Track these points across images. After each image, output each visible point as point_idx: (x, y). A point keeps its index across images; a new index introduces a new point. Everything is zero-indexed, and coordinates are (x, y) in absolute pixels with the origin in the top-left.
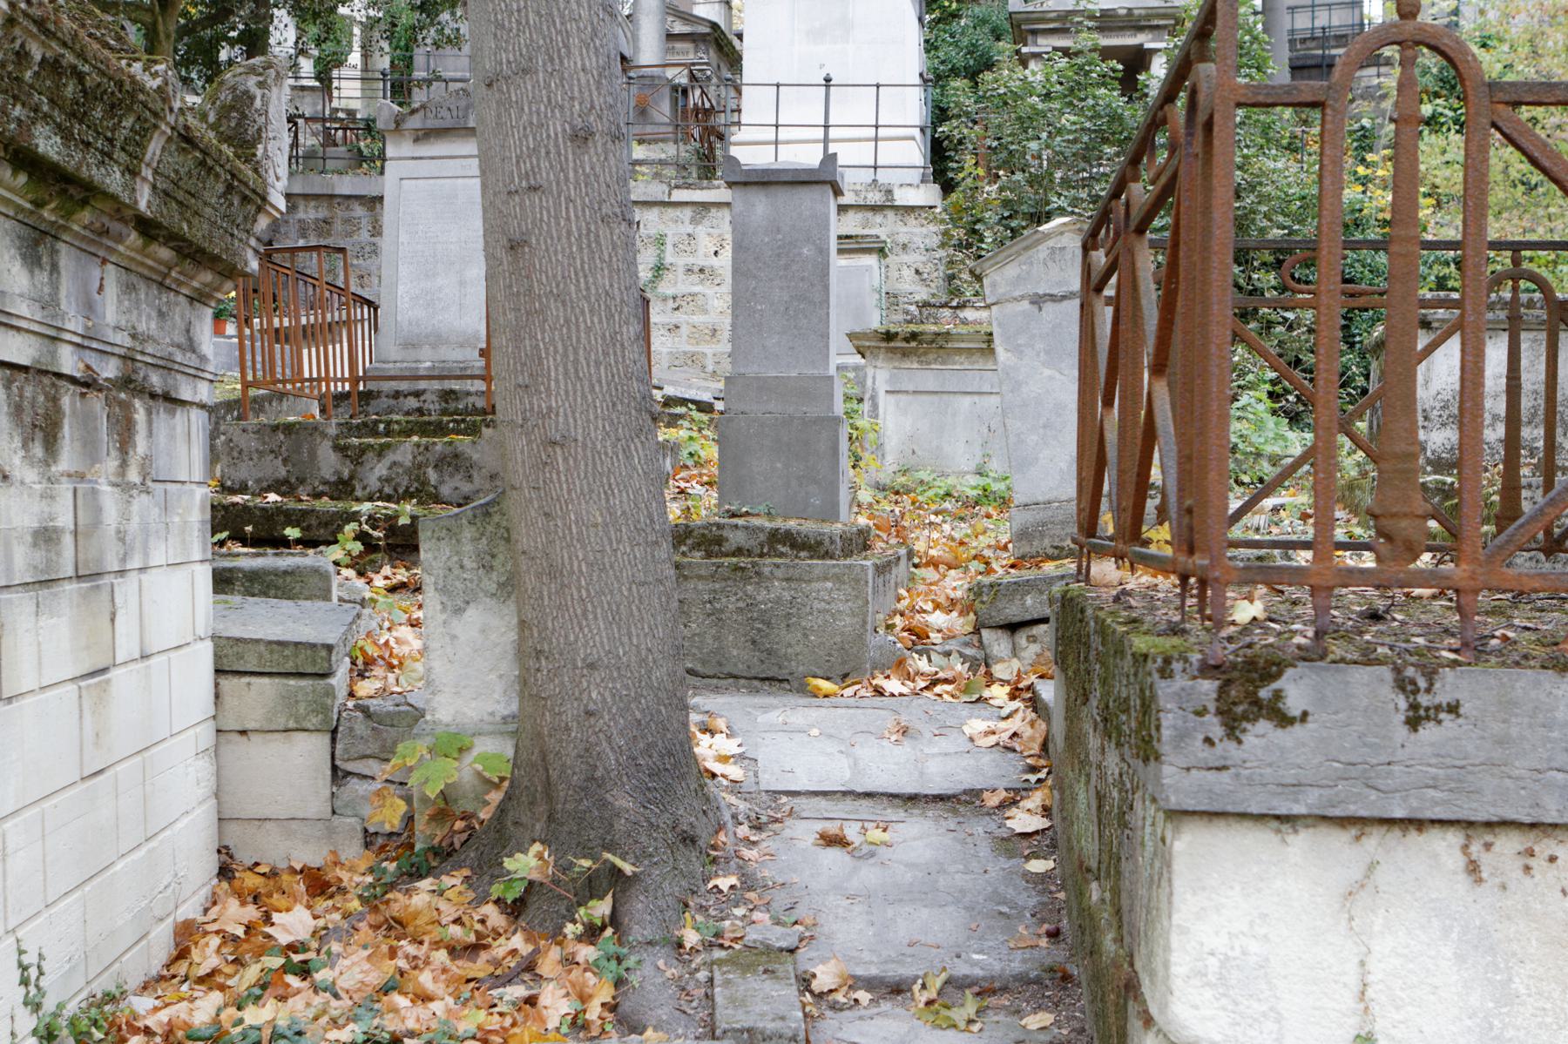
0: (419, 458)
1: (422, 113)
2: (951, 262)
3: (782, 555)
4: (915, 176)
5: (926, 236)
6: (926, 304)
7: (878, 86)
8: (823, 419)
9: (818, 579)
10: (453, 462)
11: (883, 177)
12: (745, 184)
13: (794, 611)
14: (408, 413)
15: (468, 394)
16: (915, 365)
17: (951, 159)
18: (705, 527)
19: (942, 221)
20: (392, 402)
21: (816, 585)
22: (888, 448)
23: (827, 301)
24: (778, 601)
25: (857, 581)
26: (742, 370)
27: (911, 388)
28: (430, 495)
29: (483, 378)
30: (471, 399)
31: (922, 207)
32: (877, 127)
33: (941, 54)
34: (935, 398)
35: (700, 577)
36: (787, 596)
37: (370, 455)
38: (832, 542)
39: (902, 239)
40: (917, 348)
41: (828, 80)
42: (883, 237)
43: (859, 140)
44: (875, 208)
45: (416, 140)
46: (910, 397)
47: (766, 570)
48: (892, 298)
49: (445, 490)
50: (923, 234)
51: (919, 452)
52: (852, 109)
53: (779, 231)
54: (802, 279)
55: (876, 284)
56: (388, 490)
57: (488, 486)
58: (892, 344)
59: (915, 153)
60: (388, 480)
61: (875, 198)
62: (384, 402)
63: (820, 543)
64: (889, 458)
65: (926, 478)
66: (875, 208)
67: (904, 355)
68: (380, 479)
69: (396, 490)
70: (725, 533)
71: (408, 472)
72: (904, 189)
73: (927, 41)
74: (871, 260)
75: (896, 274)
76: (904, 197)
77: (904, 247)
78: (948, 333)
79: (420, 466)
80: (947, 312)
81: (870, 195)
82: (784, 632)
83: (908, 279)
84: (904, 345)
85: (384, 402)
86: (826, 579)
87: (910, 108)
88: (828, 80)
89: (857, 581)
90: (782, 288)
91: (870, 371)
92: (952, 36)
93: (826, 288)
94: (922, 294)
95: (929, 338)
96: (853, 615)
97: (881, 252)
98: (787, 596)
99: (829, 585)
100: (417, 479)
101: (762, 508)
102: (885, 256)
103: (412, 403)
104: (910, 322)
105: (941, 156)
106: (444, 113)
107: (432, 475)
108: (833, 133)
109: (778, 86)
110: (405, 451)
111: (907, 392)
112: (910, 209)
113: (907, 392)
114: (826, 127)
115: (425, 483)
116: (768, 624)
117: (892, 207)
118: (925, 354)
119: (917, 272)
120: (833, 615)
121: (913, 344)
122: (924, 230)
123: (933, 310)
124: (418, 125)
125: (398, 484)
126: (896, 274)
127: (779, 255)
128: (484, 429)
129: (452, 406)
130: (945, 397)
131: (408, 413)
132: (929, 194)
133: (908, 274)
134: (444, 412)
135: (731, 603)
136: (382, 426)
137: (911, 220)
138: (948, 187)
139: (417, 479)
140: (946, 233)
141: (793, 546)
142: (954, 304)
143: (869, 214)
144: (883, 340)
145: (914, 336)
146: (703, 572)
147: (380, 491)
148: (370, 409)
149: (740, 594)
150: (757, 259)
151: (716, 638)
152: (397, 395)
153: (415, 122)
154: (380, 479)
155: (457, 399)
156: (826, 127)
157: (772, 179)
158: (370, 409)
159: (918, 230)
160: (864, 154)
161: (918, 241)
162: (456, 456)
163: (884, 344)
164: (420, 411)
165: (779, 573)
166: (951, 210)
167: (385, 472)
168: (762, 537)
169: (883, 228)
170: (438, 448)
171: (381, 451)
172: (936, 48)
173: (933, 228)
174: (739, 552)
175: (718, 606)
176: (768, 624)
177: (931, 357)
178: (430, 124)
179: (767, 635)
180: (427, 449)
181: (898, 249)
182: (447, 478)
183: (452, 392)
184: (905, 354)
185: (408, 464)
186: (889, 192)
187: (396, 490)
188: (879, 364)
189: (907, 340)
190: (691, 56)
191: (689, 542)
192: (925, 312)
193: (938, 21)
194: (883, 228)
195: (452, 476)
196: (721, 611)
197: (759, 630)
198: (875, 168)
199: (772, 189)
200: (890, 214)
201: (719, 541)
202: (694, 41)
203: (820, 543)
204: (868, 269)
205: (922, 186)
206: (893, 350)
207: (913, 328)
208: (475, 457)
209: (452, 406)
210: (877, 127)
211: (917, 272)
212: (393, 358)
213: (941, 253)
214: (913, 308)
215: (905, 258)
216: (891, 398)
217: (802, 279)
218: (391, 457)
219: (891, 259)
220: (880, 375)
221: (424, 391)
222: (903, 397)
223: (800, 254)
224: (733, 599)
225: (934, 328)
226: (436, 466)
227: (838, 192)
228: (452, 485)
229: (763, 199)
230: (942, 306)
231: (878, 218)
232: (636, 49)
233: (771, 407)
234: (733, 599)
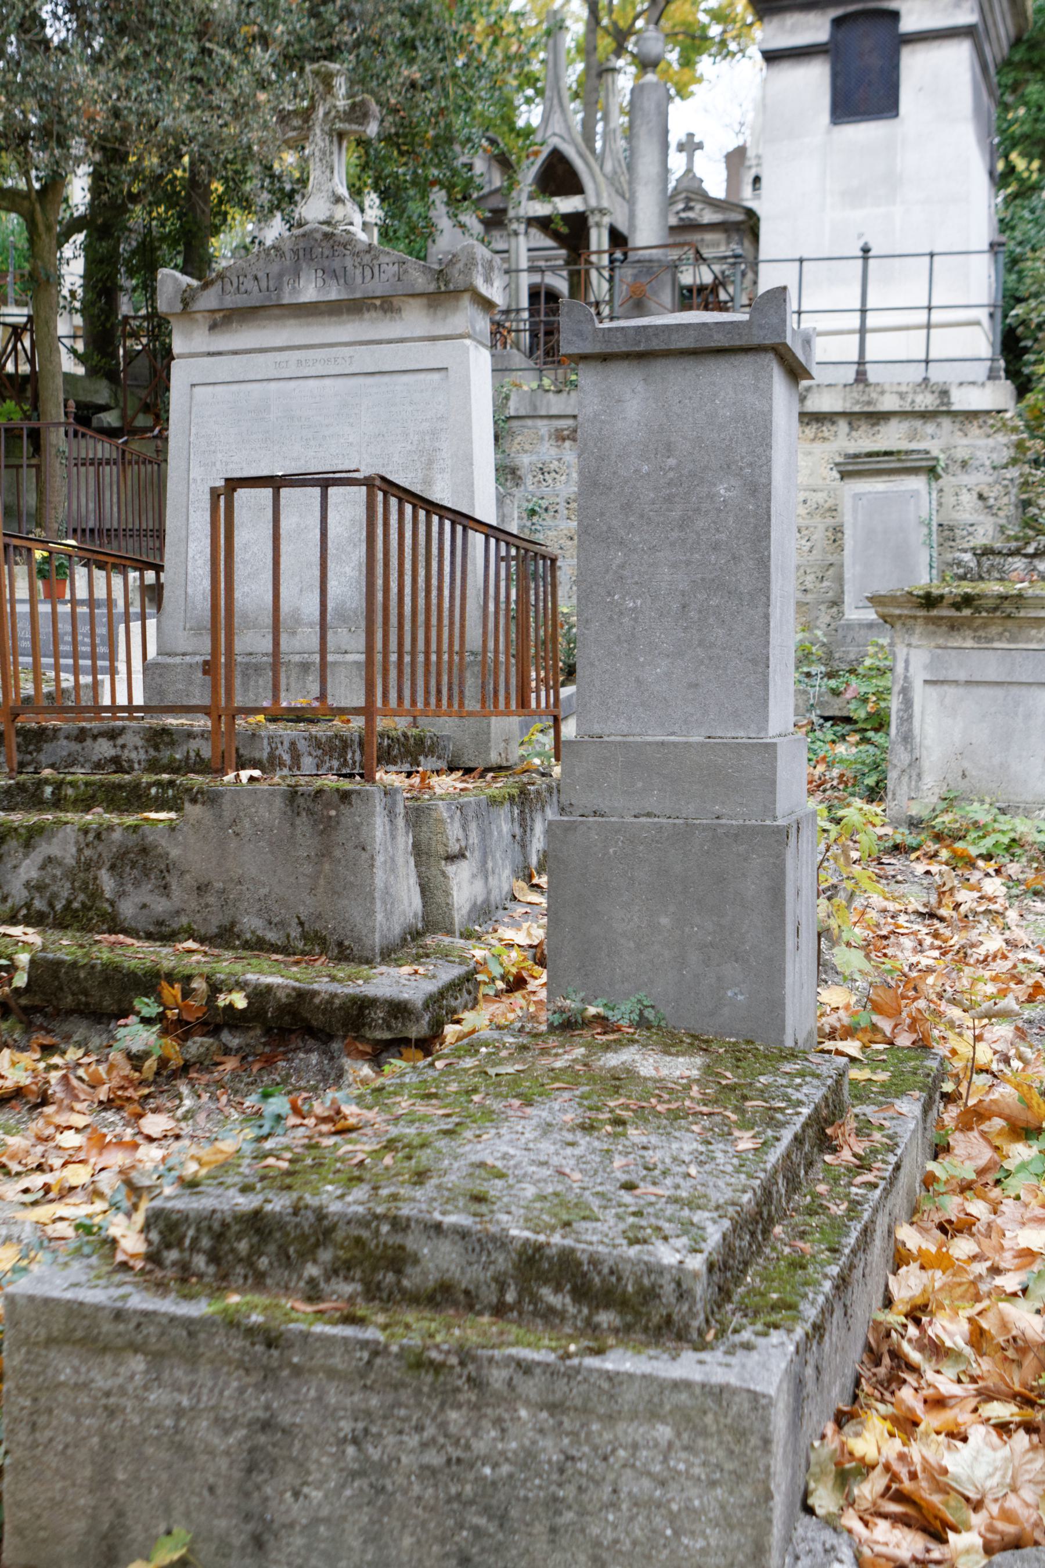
0: (87, 852)
1: (218, 286)
2: (1026, 483)
3: (550, 1315)
4: (981, 371)
5: (993, 450)
6: (988, 551)
7: (932, 255)
8: (754, 831)
9: (634, 1416)
10: (139, 859)
11: (938, 374)
12: (605, 358)
13: (568, 1492)
14: (98, 766)
15: (190, 735)
16: (969, 643)
17: (1026, 350)
18: (363, 1222)
19: (1015, 430)
20: (75, 747)
21: (630, 1431)
22: (926, 764)
23: (764, 591)
24: (528, 1459)
25: (741, 1434)
26: (597, 729)
27: (962, 676)
28: (103, 916)
29: (206, 710)
30: (194, 744)
31: (988, 412)
32: (930, 308)
33: (1018, 234)
34: (999, 692)
35: (332, 1374)
36: (550, 1450)
37: (12, 844)
38: (682, 1294)
39: (961, 454)
40: (972, 618)
41: (866, 250)
42: (935, 453)
43: (907, 328)
44: (925, 415)
45: (213, 327)
46: (961, 691)
47: (497, 1377)
48: (947, 532)
49: (127, 909)
50: (988, 447)
51: (972, 772)
52: (898, 290)
53: (669, 449)
54: (716, 547)
55: (924, 514)
56: (39, 904)
57: (194, 905)
58: (934, 613)
59: (980, 342)
60: (39, 887)
61: (926, 401)
62: (64, 747)
63: (650, 1295)
64: (929, 780)
65: (984, 818)
66: (925, 415)
67: (952, 628)
68: (27, 885)
69: (51, 905)
70: (412, 1242)
71: (70, 875)
72: (964, 389)
73: (1001, 221)
74: (917, 483)
75: (953, 500)
76: (964, 399)
77: (964, 464)
78: (1020, 596)
79: (88, 866)
80: (1018, 563)
81: (919, 398)
82: (541, 1545)
83: (968, 507)
84: (953, 613)
85: (64, 747)
86: (654, 1415)
87: (976, 282)
88: (866, 250)
89: (741, 1434)
90: (674, 565)
91: (901, 651)
92: (1032, 211)
93: (764, 563)
94: (985, 534)
95: (991, 603)
96: (727, 1523)
97: (932, 472)
98: (550, 1450)
99: (664, 1432)
100: (84, 888)
101: (623, 1013)
102: (938, 477)
103: (104, 749)
104: (963, 578)
105: (1013, 348)
106: (249, 284)
107: (107, 883)
108: (872, 320)
109: (801, 261)
110: (67, 832)
111: (956, 682)
112: (972, 415)
113: (956, 682)
114: (863, 311)
115: (96, 894)
116: (503, 1520)
117: (949, 413)
118: (985, 626)
119: (981, 497)
120: (673, 1518)
121: (967, 612)
122: (991, 442)
123: (998, 560)
124: (214, 304)
125: (54, 896)
126: (953, 500)
127: (669, 499)
128: (187, 805)
129: (165, 754)
130: (1014, 690)
131: (98, 766)
132: (997, 395)
133: (968, 499)
134: (153, 766)
135: (406, 1450)
136: (48, 790)
137: (974, 430)
138: (1023, 387)
139: (84, 888)
140: (1019, 446)
141: (582, 1293)
142: (1030, 550)
143: (918, 423)
144: (921, 606)
145: (967, 600)
146: (337, 1362)
147: (28, 905)
148: (42, 758)
149: (430, 1431)
150: (627, 508)
151: (372, 1537)
152: (81, 736)
153: (209, 300)
154: (27, 885)
155: (172, 744)
156: (863, 311)
157: (656, 345)
158: (42, 758)
159: (982, 442)
160: (912, 345)
161: (983, 456)
162: (144, 851)
163: (922, 613)
164: (117, 764)
165: (530, 1387)
166: (1027, 415)
167: (34, 874)
168: (502, 1262)
169: (934, 440)
170: (117, 835)
171: (31, 836)
172: (1013, 228)
173: (1002, 438)
174: (441, 1296)
175: (374, 1453)
176: (503, 1520)
177: (994, 630)
178: (232, 301)
179: (498, 1549)
180: (98, 836)
181: (955, 468)
182: (129, 888)
183: (165, 731)
184: (954, 626)
185: (70, 861)
186: (945, 393)
187: (51, 905)
188: (915, 640)
189: (956, 606)
190: (723, 248)
191: (326, 1255)
192: (986, 563)
193: (1016, 196)
194: (934, 440)
195: (137, 884)
196: (384, 1468)
197: (478, 1533)
198: (927, 362)
199: (658, 367)
200: (946, 422)
201: (398, 1260)
202: (726, 231)
203: (650, 1295)
204: (915, 494)
205: (989, 384)
206: (936, 621)
207: (967, 587)
208: (175, 853)
209: (165, 754)
210: (930, 308)
211: (981, 497)
212: (181, 649)
213: (1013, 473)
214: (967, 557)
215: (966, 479)
216: (933, 692)
217: (716, 547)
218: (44, 849)
219: (946, 481)
220: (915, 657)
221: (122, 730)
222: (951, 691)
223: (711, 497)
224: (413, 1441)
225: (996, 588)
226: (112, 867)
227: (796, 371)
228: (139, 900)
229: (640, 387)
230: (1011, 554)
231: (930, 428)
232: (632, 225)
233: (651, 803)
234: (413, 1441)
